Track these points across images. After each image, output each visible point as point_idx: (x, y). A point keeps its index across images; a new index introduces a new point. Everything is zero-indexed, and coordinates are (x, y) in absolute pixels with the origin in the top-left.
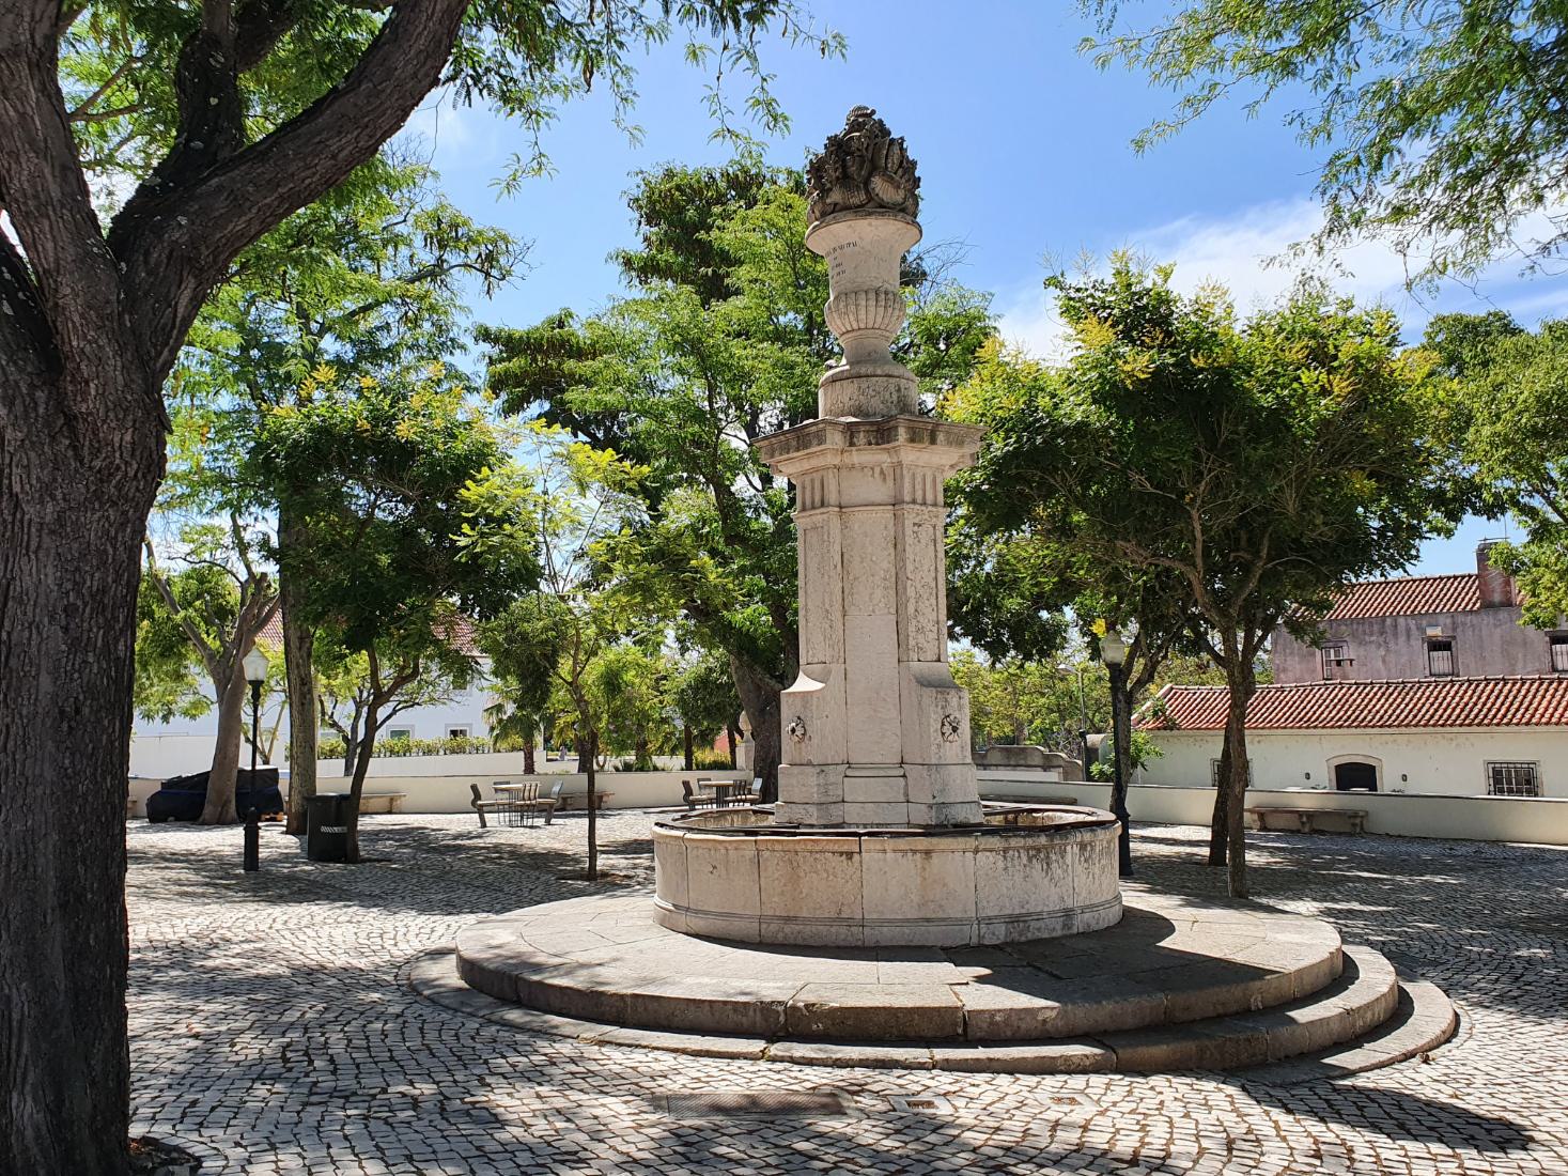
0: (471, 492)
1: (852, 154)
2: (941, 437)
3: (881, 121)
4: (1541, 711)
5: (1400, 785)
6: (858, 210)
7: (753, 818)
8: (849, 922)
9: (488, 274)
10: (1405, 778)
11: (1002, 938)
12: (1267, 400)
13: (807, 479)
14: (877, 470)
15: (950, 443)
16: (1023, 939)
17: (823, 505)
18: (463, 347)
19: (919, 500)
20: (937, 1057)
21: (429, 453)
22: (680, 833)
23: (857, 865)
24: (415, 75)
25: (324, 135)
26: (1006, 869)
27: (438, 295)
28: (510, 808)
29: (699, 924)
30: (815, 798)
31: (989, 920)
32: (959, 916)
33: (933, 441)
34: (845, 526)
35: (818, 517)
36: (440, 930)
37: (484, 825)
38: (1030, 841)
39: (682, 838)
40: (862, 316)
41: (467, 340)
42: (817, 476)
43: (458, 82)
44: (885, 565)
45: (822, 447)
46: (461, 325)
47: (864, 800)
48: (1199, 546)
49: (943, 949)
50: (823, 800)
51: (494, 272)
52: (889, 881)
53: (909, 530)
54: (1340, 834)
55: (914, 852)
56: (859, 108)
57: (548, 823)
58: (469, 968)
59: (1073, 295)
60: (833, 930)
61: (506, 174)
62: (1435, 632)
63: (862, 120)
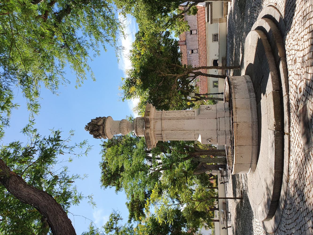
0: (160, 221)
1: (93, 129)
2: (149, 110)
3: (88, 124)
4: (203, 34)
5: (217, 56)
6: (104, 128)
7: (229, 155)
8: (253, 125)
9: (118, 219)
10: (216, 55)
11: (254, 93)
12: (146, 60)
13: (156, 138)
14: (155, 123)
15: (150, 109)
16: (254, 89)
17: (161, 134)
18: (132, 226)
19: (161, 113)
20: (286, 94)
21: (152, 231)
22: (234, 165)
23: (240, 123)
24: (48, 200)
25: (57, 224)
26: (239, 93)
27: (122, 230)
28: (227, 221)
29: (254, 161)
30: (225, 136)
31: (250, 96)
32: (249, 102)
33: (149, 112)
34: (166, 130)
35: (164, 135)
36: (257, 229)
37: (231, 227)
38: (232, 88)
39: (235, 165)
40: (125, 125)
41: (131, 224)
42: (156, 136)
43: (64, 205)
44: (174, 122)
45: (149, 133)
46: (128, 226)
47: (225, 126)
48: (173, 75)
49: (257, 104)
50: (225, 135)
51: (118, 218)
52: (243, 116)
53: (167, 117)
54: (226, 62)
55: (236, 111)
56: (85, 128)
57: (230, 213)
58: (269, 216)
59: (126, 96)
60: (254, 128)
61: (92, 205)
62: (190, 52)
63: (87, 128)
